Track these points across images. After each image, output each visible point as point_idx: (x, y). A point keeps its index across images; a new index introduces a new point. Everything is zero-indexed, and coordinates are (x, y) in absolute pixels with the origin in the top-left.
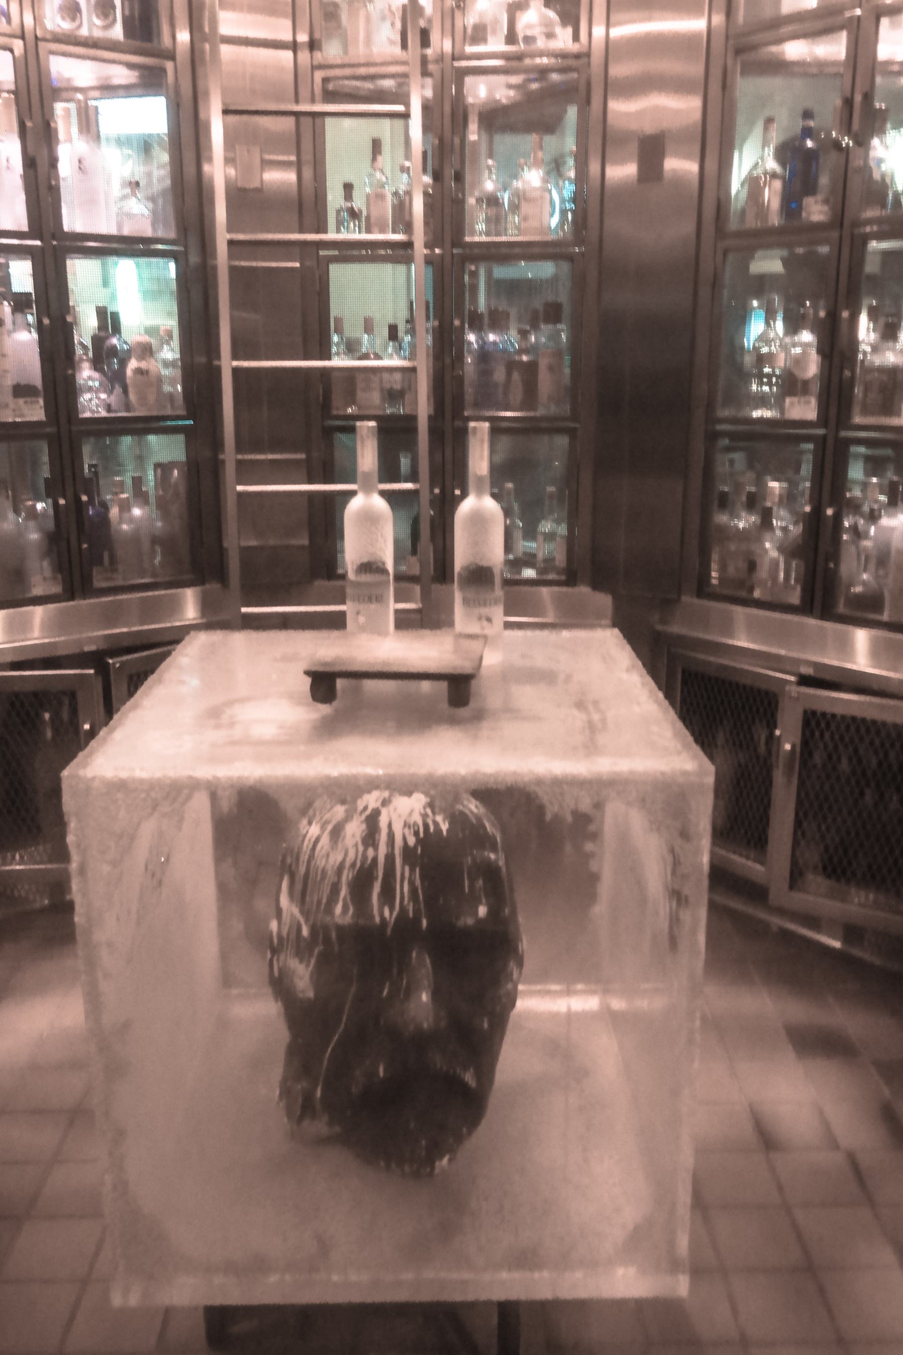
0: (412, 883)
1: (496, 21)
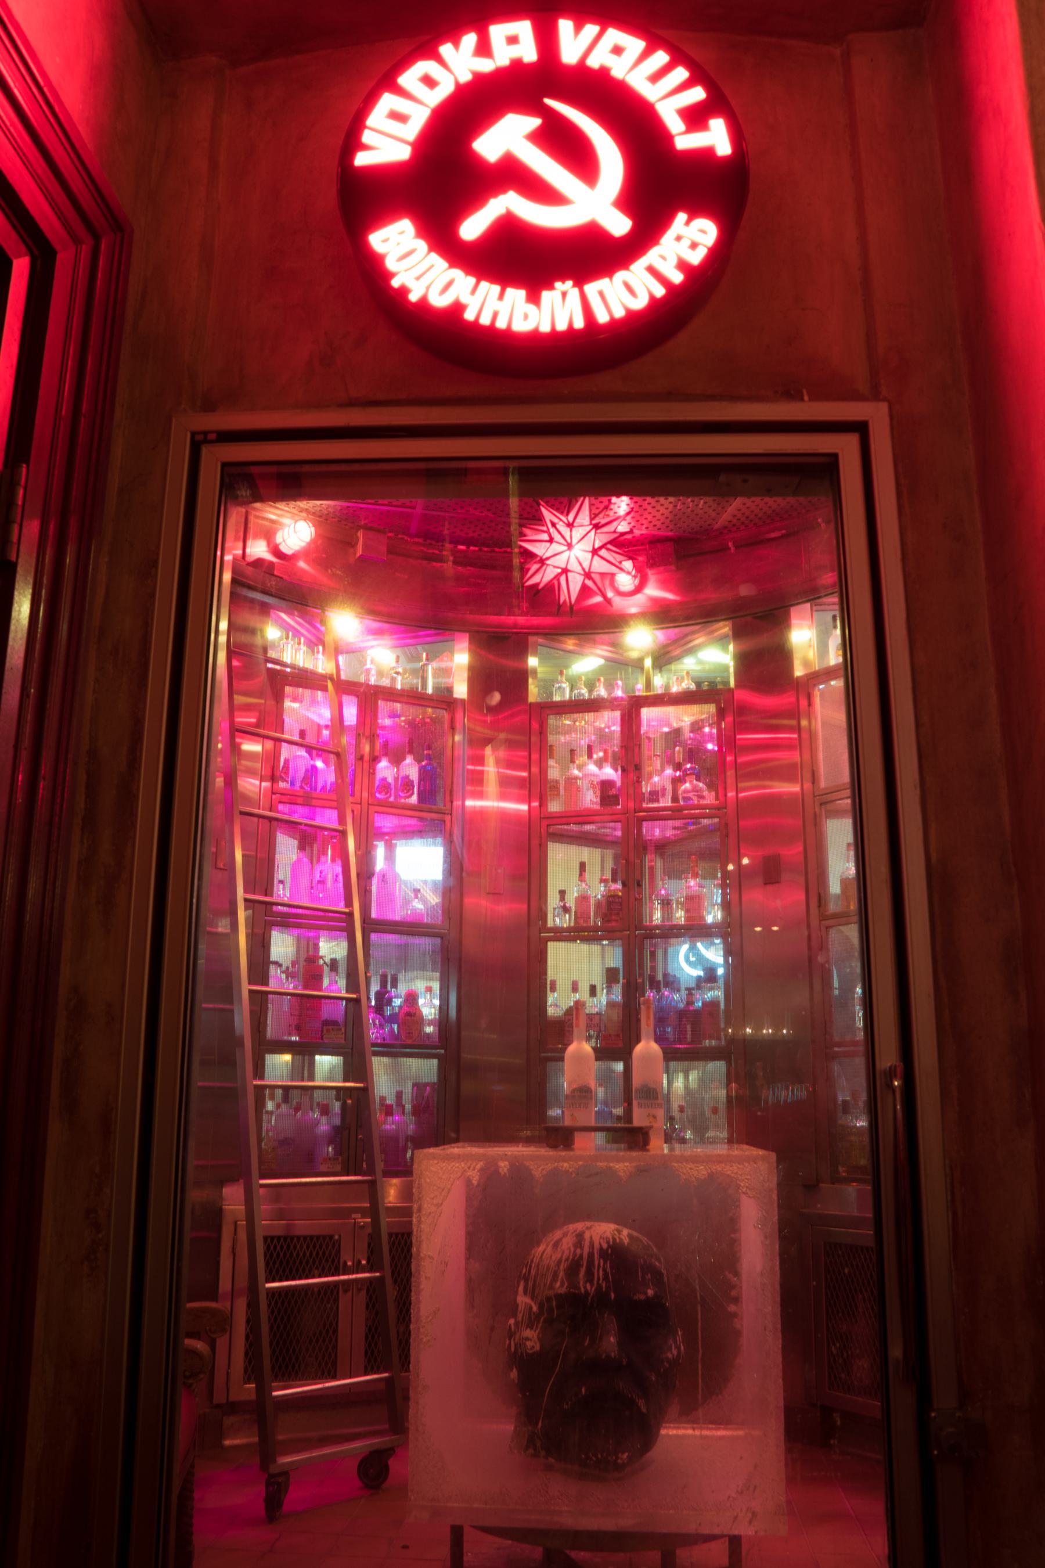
0: (604, 1270)
1: (664, 790)
